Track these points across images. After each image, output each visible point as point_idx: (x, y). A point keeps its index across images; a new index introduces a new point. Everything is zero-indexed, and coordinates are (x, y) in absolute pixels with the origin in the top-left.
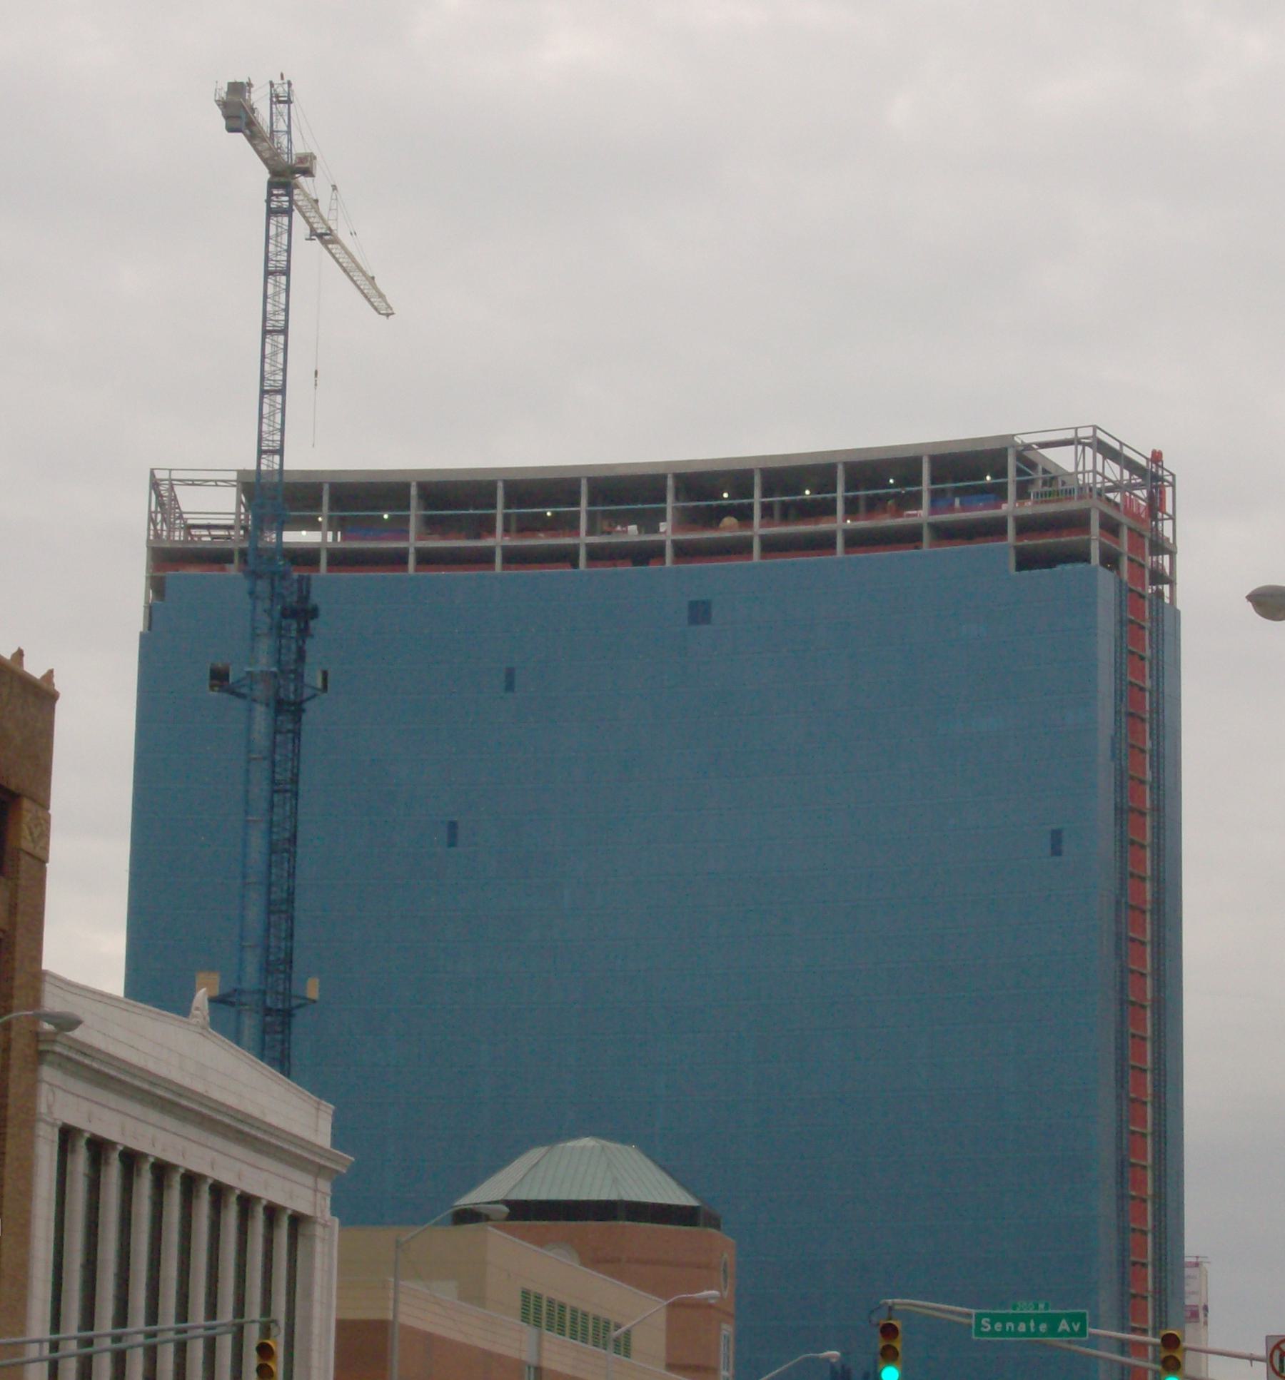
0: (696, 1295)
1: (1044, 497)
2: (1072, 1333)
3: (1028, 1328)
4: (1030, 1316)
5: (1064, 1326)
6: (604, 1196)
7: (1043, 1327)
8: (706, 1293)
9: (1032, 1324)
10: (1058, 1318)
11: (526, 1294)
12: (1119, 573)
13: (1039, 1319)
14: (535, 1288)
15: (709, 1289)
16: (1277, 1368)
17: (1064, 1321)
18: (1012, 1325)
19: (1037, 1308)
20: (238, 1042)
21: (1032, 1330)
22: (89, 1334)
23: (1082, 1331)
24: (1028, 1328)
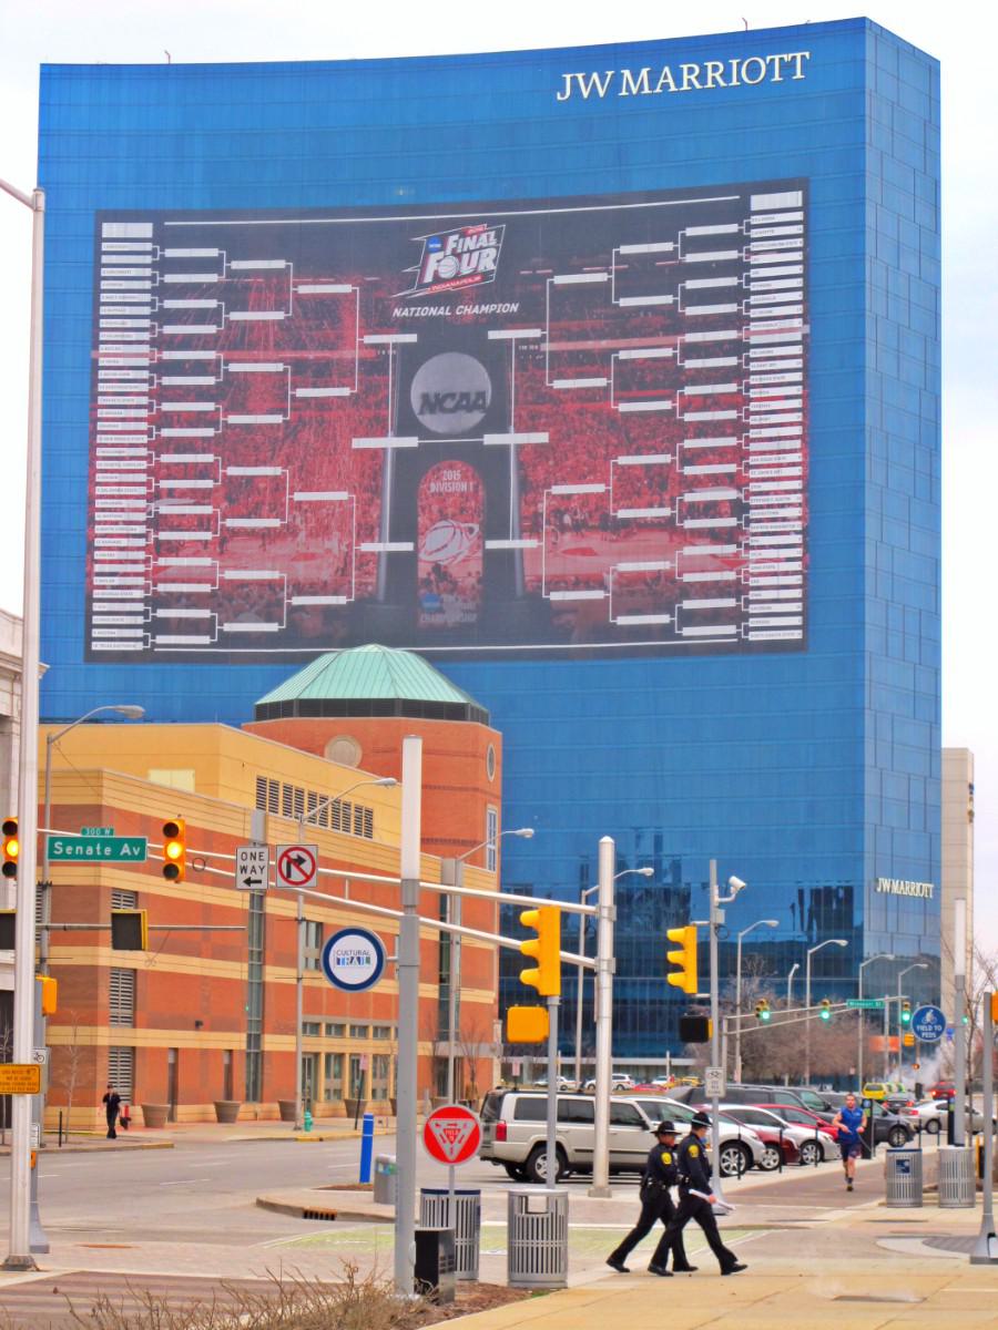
0: (518, 832)
1: (761, 1025)
2: (133, 857)
3: (95, 851)
4: (97, 840)
5: (126, 849)
6: (383, 695)
7: (108, 851)
8: (524, 830)
9: (98, 848)
10: (120, 842)
11: (261, 782)
12: (460, 261)
13: (105, 842)
14: (270, 776)
15: (526, 827)
16: (285, 873)
17: (126, 846)
18: (81, 848)
19: (103, 833)
20: (871, 21)
21: (99, 853)
22: (668, 1068)
23: (142, 856)
24: (95, 851)
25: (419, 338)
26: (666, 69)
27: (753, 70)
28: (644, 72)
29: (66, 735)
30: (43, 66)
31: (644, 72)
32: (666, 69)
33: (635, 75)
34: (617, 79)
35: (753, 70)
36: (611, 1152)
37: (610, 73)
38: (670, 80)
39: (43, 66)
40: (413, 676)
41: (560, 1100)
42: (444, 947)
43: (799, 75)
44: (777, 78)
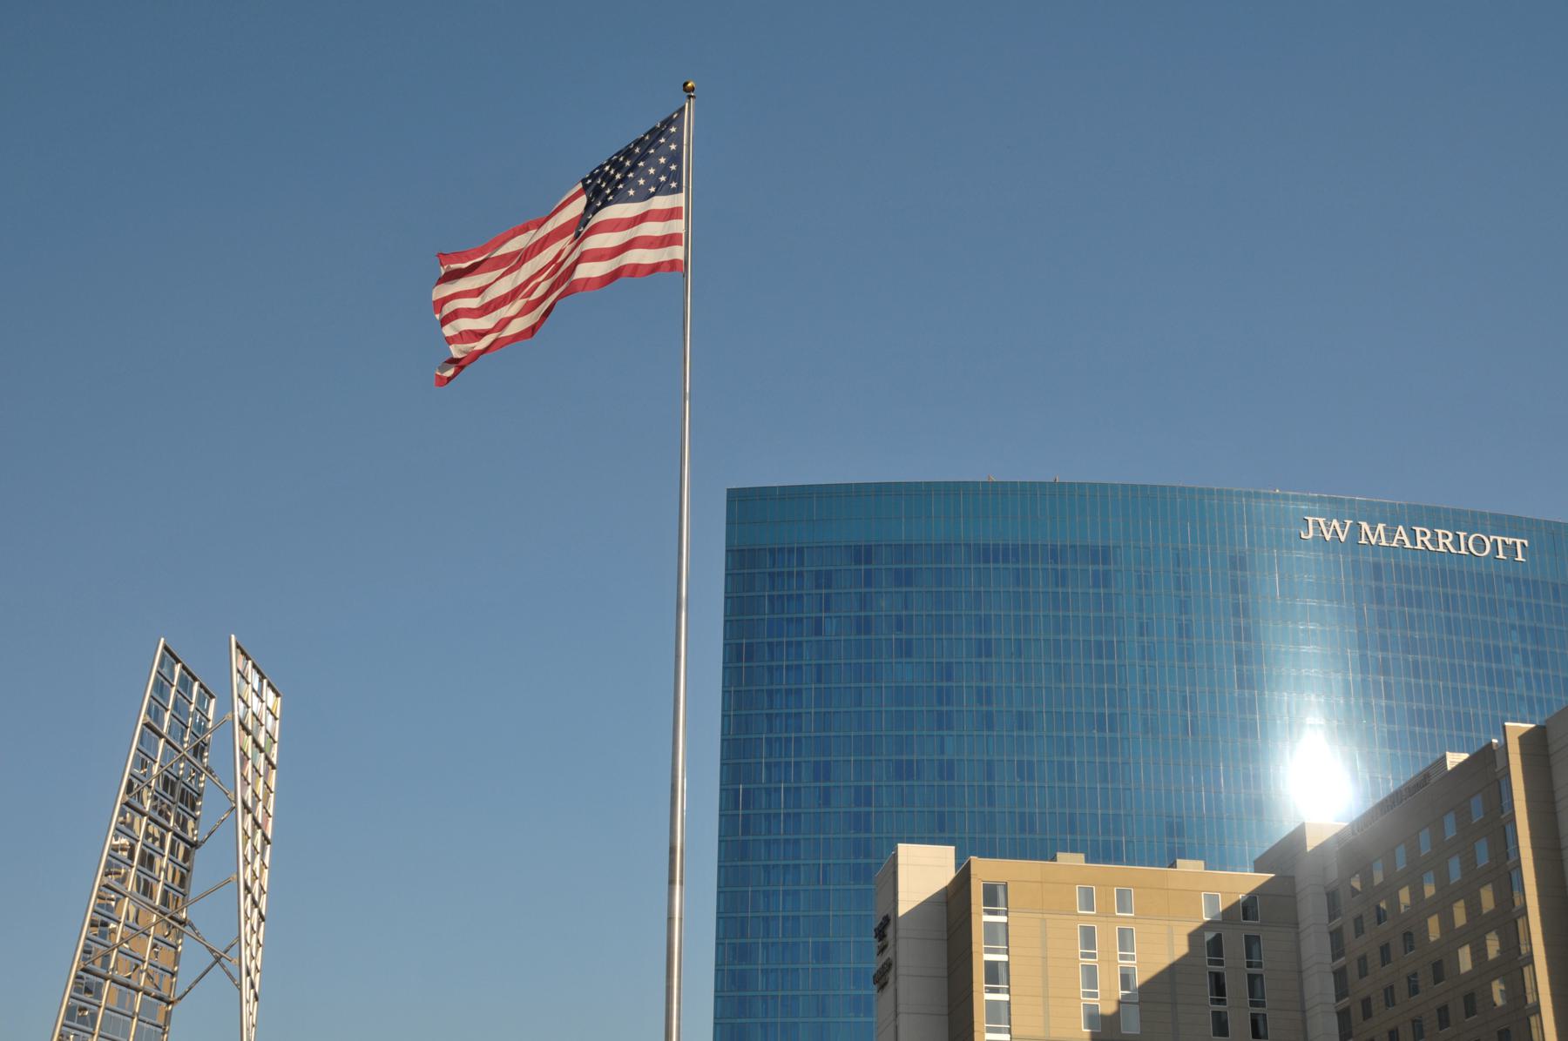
11: (1226, 1034)
25: (1502, 1007)
26: (1401, 528)
27: (1480, 544)
28: (1381, 527)
29: (901, 1000)
30: (729, 490)
31: (1381, 527)
32: (1401, 528)
33: (1373, 530)
34: (1356, 528)
35: (1480, 544)
36: (1006, 886)
37: (1349, 522)
38: (1405, 537)
39: (729, 490)
40: (1198, 791)
41: (987, 962)
42: (1260, 1019)
43: (1520, 558)
44: (1501, 556)
